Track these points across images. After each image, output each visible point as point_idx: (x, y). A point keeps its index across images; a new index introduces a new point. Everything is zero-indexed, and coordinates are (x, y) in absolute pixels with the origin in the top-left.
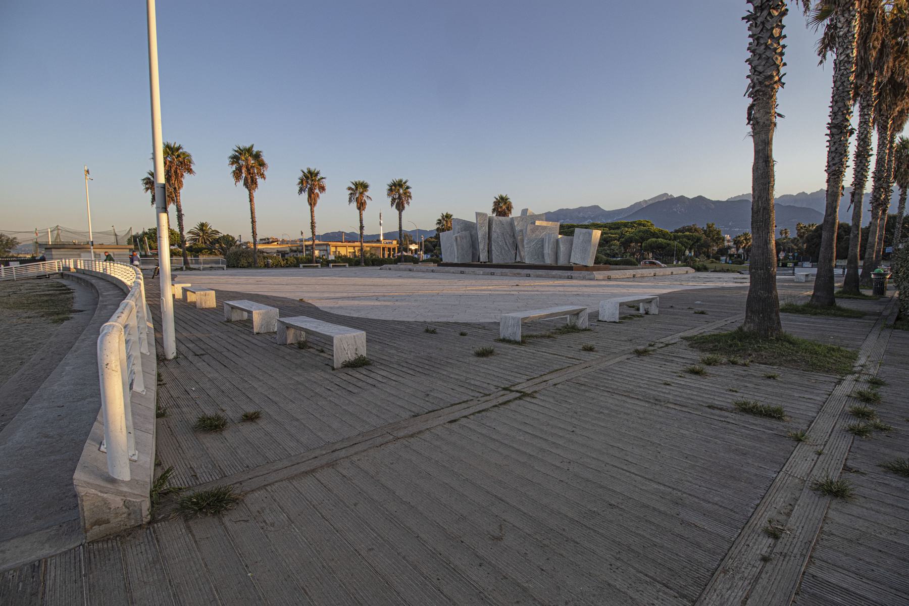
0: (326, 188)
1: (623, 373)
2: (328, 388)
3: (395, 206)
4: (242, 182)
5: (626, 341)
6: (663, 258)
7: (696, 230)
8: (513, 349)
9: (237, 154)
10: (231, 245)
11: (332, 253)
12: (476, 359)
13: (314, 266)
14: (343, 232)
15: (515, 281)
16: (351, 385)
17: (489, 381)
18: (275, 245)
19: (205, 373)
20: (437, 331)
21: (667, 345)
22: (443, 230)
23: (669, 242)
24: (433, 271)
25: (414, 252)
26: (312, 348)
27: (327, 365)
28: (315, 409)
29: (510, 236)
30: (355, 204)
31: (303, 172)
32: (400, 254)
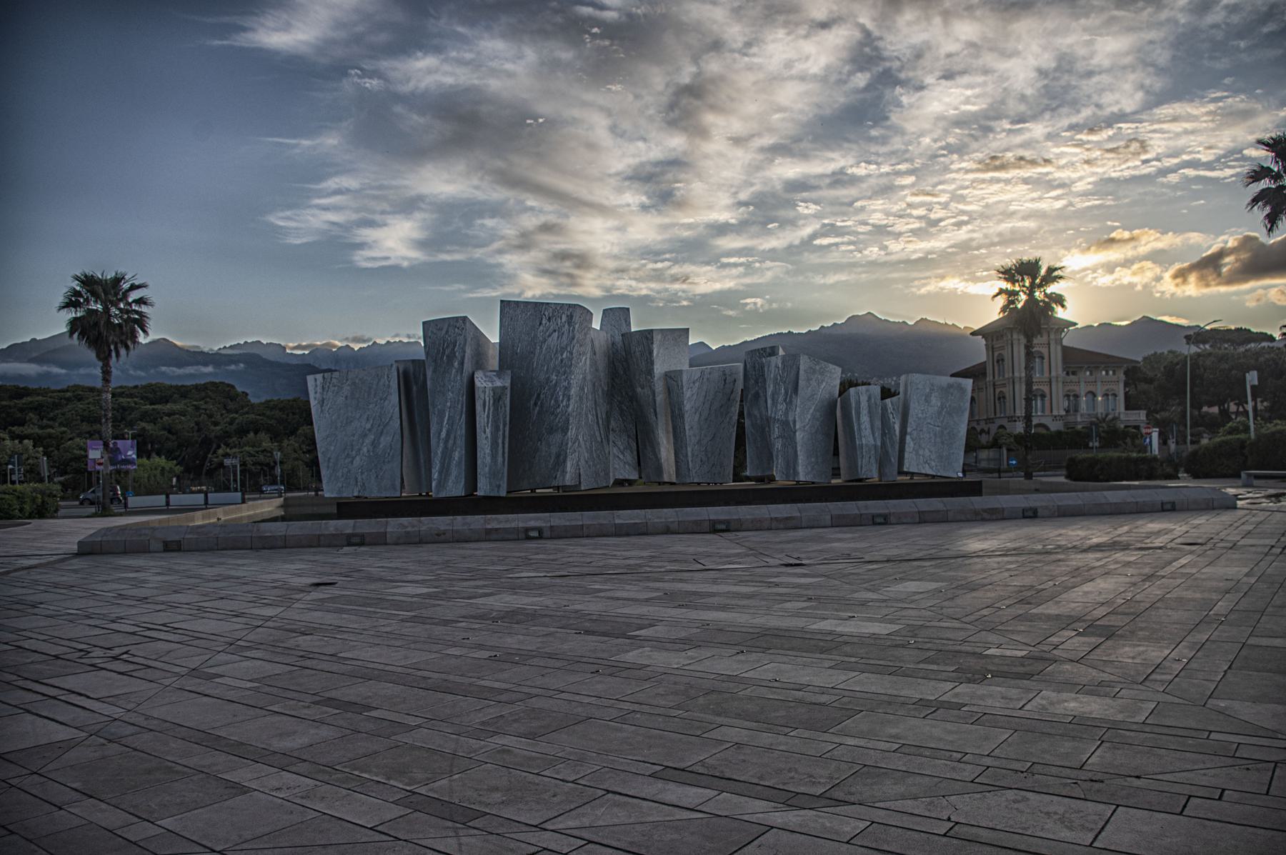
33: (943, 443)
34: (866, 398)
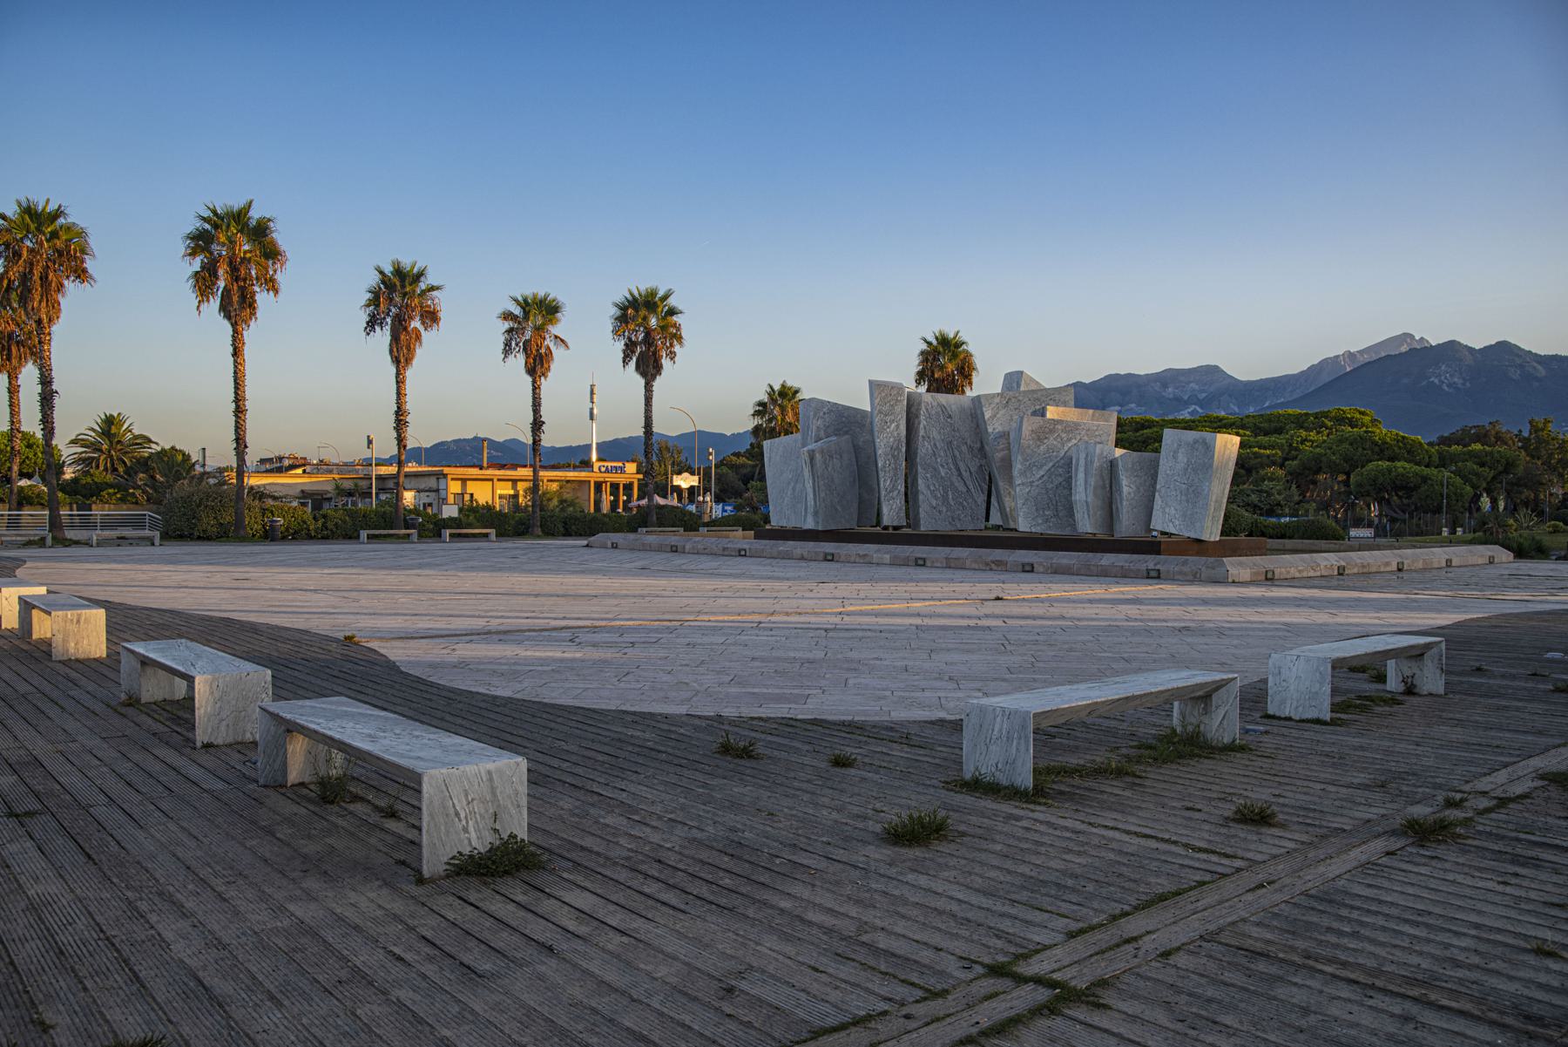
0: (442, 315)
1: (1385, 910)
2: (396, 950)
3: (633, 364)
4: (215, 303)
5: (1366, 787)
6: (1411, 517)
7: (1499, 438)
8: (1010, 817)
9: (207, 226)
10: (178, 477)
11: (451, 499)
12: (888, 852)
13: (398, 537)
14: (484, 440)
15: (987, 587)
16: (472, 943)
17: (936, 940)
18: (297, 476)
19: (22, 879)
20: (760, 749)
21: (1503, 802)
22: (772, 433)
23: (1426, 471)
24: (741, 553)
25: (686, 495)
26: (362, 799)
27: (403, 863)
28: (345, 1034)
29: (971, 448)
30: (521, 358)
31: (381, 272)
32: (644, 502)
33: (1188, 501)
34: (1084, 456)
